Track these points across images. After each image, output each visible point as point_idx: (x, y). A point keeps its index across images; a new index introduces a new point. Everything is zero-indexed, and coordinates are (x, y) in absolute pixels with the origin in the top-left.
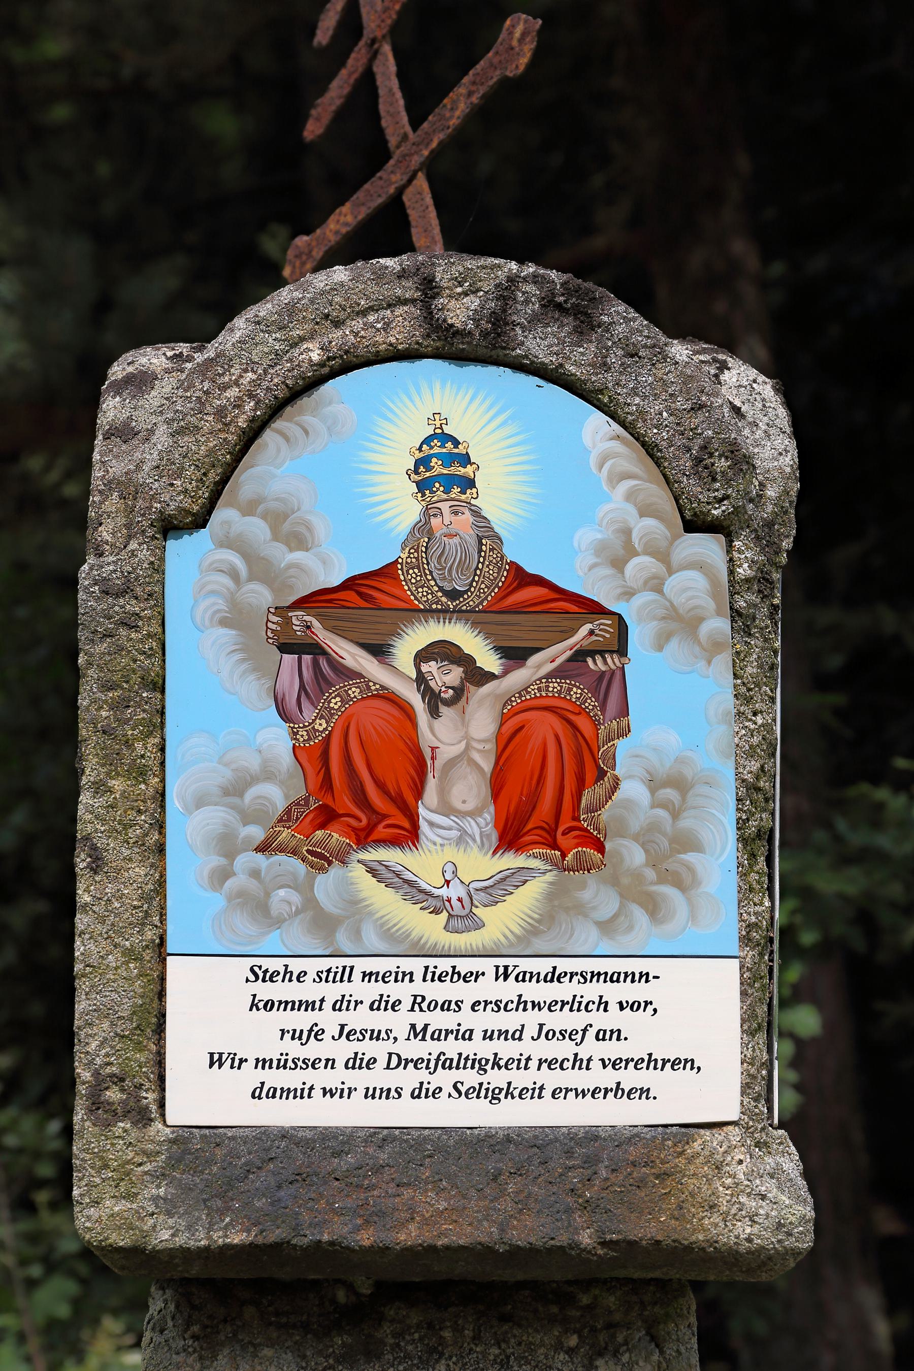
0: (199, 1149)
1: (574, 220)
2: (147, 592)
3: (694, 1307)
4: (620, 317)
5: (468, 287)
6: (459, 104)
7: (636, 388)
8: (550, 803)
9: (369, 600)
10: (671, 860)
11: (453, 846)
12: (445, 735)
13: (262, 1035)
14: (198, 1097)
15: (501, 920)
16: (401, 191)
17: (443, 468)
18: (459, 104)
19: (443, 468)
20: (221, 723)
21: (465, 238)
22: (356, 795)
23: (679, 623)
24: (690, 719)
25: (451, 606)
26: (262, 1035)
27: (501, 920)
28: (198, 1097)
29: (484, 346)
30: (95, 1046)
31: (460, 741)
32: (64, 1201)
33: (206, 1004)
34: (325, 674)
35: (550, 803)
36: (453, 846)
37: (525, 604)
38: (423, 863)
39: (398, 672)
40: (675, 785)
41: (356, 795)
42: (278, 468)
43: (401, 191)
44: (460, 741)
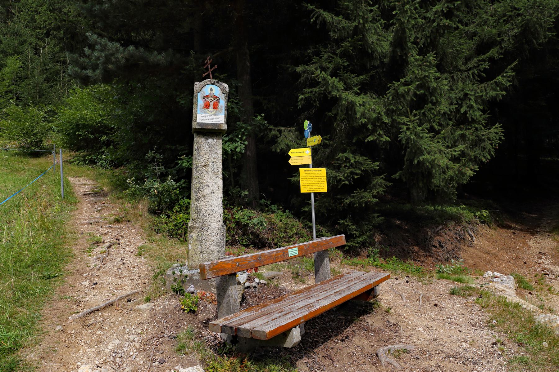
0: (198, 123)
1: (219, 76)
2: (197, 95)
3: (321, 11)
4: (220, 83)
5: (213, 81)
6: (213, 69)
7: (221, 86)
8: (215, 107)
9: (207, 96)
10: (221, 110)
11: (211, 109)
12: (211, 103)
13: (202, 118)
14: (198, 121)
15: (213, 113)
16: (378, 283)
17: (211, 90)
18: (213, 69)
19: (211, 90)
20: (200, 102)
21: (213, 78)
22: (207, 106)
23: (222, 98)
24: (223, 103)
25: (211, 97)
26: (202, 118)
27: (213, 113)
28: (198, 121)
29: (214, 84)
30: (194, 118)
31: (212, 104)
32: (370, 56)
33: (199, 116)
34: (205, 100)
35: (215, 107)
36: (211, 109)
37: (215, 97)
38: (209, 110)
39: (209, 100)
40: (222, 106)
41: (207, 106)
42: (203, 90)
43: (378, 283)
44: (212, 104)
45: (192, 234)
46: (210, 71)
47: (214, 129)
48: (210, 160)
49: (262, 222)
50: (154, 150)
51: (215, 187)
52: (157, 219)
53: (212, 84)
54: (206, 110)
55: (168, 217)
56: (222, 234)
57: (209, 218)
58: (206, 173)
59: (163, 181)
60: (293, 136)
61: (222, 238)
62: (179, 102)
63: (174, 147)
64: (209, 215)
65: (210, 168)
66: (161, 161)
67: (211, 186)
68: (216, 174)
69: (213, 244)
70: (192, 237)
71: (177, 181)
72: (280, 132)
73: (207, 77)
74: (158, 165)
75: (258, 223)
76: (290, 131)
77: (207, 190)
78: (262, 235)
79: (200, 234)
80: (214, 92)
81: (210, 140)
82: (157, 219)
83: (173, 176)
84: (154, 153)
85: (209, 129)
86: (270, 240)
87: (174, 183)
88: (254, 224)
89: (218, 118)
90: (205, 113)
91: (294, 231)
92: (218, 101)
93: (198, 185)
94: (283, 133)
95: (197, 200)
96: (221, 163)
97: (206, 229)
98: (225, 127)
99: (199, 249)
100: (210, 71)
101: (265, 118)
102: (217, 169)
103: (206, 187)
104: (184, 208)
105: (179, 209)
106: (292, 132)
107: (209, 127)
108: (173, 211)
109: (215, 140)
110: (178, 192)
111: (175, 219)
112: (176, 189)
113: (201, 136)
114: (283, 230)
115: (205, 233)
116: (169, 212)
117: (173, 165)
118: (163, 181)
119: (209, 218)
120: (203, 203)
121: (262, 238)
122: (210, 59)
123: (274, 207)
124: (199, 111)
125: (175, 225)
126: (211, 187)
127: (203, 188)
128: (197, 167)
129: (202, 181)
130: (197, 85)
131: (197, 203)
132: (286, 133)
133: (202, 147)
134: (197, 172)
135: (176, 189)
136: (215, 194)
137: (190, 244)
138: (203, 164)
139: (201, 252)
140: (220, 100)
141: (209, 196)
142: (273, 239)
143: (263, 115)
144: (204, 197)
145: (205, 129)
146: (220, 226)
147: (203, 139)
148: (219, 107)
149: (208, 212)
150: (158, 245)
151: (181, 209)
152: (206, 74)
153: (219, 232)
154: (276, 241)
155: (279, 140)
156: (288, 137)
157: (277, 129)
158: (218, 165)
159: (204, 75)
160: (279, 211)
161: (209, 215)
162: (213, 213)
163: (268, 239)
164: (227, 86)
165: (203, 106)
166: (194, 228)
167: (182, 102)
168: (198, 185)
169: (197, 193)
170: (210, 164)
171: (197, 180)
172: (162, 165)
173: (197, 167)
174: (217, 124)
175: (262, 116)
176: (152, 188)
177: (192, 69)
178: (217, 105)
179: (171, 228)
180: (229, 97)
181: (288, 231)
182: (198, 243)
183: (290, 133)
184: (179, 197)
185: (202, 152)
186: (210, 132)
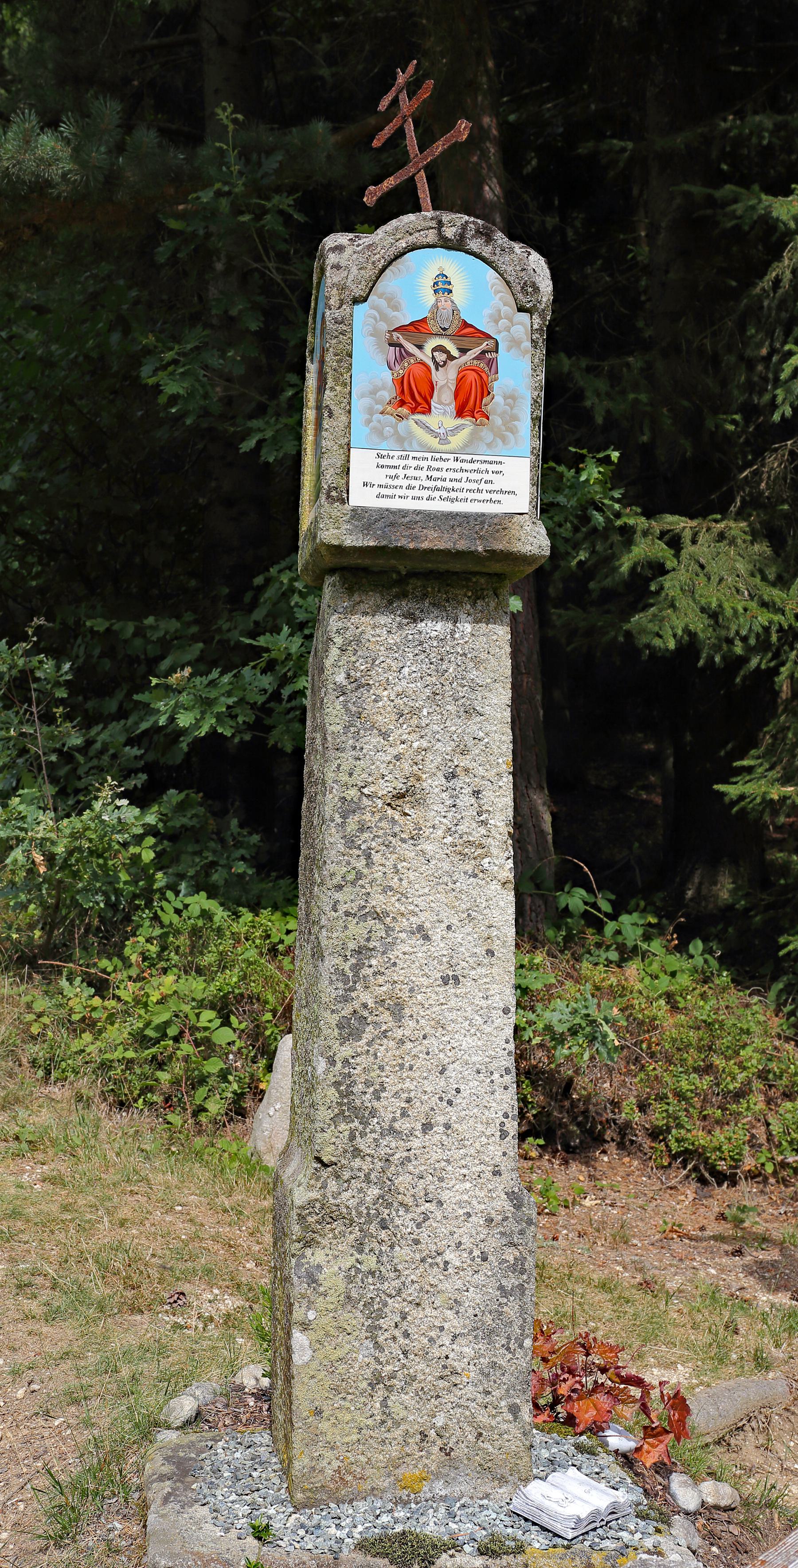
0: (358, 514)
2: (346, 322)
5: (454, 222)
6: (439, 147)
7: (503, 261)
8: (471, 402)
9: (417, 329)
10: (511, 420)
11: (442, 413)
12: (436, 378)
13: (380, 477)
14: (360, 497)
15: (456, 441)
17: (442, 286)
18: (439, 147)
19: (442, 286)
22: (414, 396)
23: (515, 343)
24: (518, 377)
25: (443, 332)
26: (380, 477)
27: (456, 441)
28: (360, 497)
29: (457, 245)
31: (445, 380)
33: (363, 465)
34: (404, 355)
35: (471, 402)
36: (442, 413)
37: (467, 334)
39: (425, 356)
40: (512, 398)
41: (414, 396)
42: (389, 282)
44: (445, 380)
45: (316, 1256)
46: (416, 170)
47: (460, 555)
48: (432, 762)
49: (593, 1022)
50: (25, 638)
51: (466, 940)
52: (41, 1004)
53: (446, 244)
54: (412, 423)
55: (101, 986)
56: (510, 1255)
57: (430, 1148)
58: (407, 850)
59: (71, 796)
60: (742, 567)
61: (511, 1282)
62: (157, 389)
63: (130, 628)
64: (427, 1127)
65: (435, 813)
66: (61, 693)
67: (437, 934)
68: (469, 851)
69: (454, 1323)
70: (312, 1280)
71: (140, 799)
72: (674, 542)
73: (403, 201)
74: (48, 719)
75: (574, 1031)
76: (721, 536)
77: (412, 964)
78: (582, 1083)
79: (371, 1262)
80: (459, 296)
81: (433, 627)
82: (41, 1004)
83: (125, 774)
84: (27, 654)
85: (430, 553)
86: (629, 1112)
87: (129, 813)
88: (548, 1028)
89: (495, 481)
90: (403, 441)
91: (755, 1063)
92: (488, 358)
93: (357, 930)
94: (688, 549)
95: (350, 1029)
96: (507, 781)
97: (404, 1221)
98: (535, 540)
99: (364, 1355)
100: (416, 170)
101: (616, 477)
102: (482, 818)
103: (407, 944)
104: (183, 941)
105: (153, 949)
106: (732, 542)
107: (433, 540)
108: (125, 961)
109: (468, 627)
110: (148, 856)
111: (137, 1001)
112: (138, 840)
113: (374, 599)
114: (692, 1057)
115: (402, 1252)
116: (104, 963)
117: (112, 705)
118: (71, 796)
119: (430, 1148)
120: (386, 1050)
121: (587, 1099)
122: (413, 88)
123: (630, 926)
124: (359, 432)
125: (141, 1040)
126: (439, 946)
127: (389, 946)
128: (348, 809)
129: (378, 901)
130: (344, 254)
131: (346, 1051)
132: (703, 549)
133: (378, 675)
134: (350, 842)
135: (138, 840)
136: (467, 985)
137: (305, 1326)
138: (384, 788)
139: (377, 1380)
140: (504, 358)
141: (429, 1000)
142: (643, 1107)
143: (615, 455)
144: (397, 1010)
145: (400, 552)
146: (503, 1203)
147: (382, 619)
148: (497, 402)
149: (418, 1110)
150: (55, 1180)
151: (164, 948)
152: (390, 183)
153: (493, 1243)
154: (657, 1117)
155: (671, 585)
156: (713, 567)
157: (656, 526)
158: (488, 795)
159: (371, 196)
160: (656, 946)
161: (427, 1127)
162: (453, 1114)
163: (616, 1105)
164: (537, 262)
165: (388, 393)
166: (331, 1216)
167: (172, 388)
168: (357, 930)
169: (351, 981)
170: (434, 784)
171: (347, 899)
172: (68, 717)
173: (348, 809)
174: (481, 518)
175: (607, 460)
176: (19, 841)
177: (224, 204)
178: (485, 390)
179: (118, 1054)
180: (567, 338)
181: (718, 1061)
182: (355, 1319)
183: (723, 546)
184: (151, 879)
185: (380, 706)
186: (418, 573)
